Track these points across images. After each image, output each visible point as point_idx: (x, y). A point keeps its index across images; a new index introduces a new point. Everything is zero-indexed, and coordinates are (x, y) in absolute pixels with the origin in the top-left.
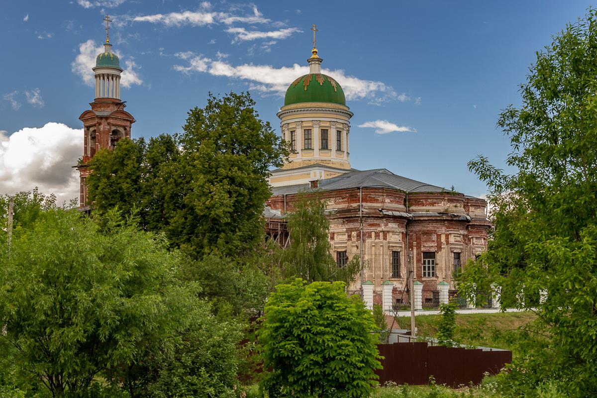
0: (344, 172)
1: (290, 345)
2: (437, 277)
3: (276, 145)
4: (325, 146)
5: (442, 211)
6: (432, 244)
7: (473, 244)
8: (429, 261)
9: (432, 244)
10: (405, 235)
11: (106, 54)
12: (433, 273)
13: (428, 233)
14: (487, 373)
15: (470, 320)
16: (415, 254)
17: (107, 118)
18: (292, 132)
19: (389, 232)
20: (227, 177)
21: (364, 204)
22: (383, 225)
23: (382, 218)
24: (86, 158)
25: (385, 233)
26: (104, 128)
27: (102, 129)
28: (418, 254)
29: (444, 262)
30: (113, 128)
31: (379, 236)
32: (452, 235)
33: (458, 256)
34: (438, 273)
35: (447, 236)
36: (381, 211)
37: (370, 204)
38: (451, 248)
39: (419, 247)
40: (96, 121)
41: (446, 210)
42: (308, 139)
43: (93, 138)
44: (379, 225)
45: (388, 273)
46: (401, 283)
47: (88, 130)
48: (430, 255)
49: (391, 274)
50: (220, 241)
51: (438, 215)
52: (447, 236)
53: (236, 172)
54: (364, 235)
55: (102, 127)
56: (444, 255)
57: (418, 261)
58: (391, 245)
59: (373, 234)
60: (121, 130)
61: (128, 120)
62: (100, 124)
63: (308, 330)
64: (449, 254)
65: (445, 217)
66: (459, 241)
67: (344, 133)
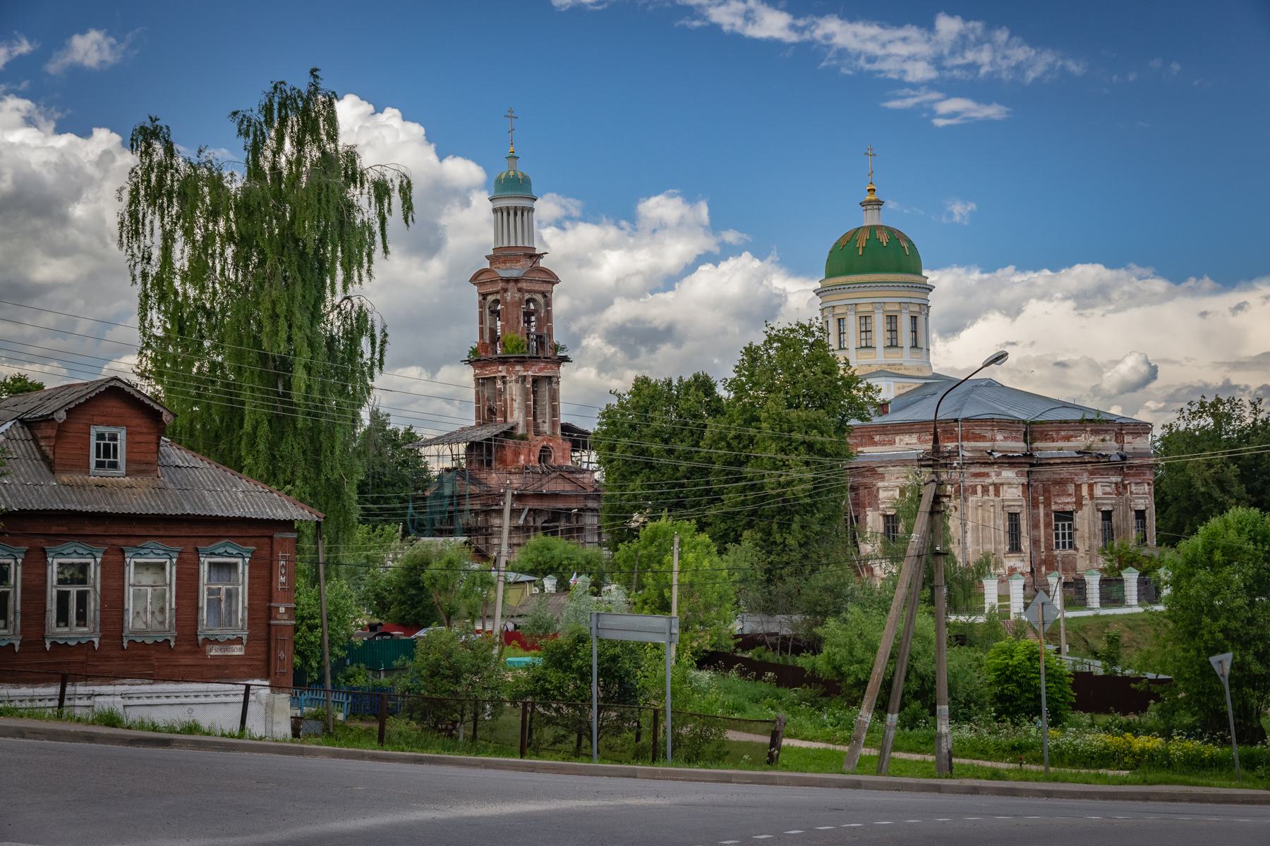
0: (924, 381)
1: (1012, 687)
2: (1076, 549)
3: (859, 390)
4: (893, 345)
5: (1082, 449)
6: (1069, 500)
7: (1131, 493)
8: (1063, 525)
9: (1069, 500)
10: (1027, 487)
11: (512, 173)
12: (1070, 544)
13: (1062, 483)
14: (1152, 702)
15: (1130, 623)
16: (1042, 514)
17: (517, 280)
18: (839, 320)
19: (1002, 484)
20: (804, 442)
21: (965, 444)
22: (993, 474)
23: (993, 464)
24: (482, 345)
25: (997, 487)
26: (513, 297)
27: (509, 298)
28: (1047, 515)
29: (1086, 526)
30: (527, 296)
31: (988, 491)
32: (1099, 485)
33: (1107, 515)
34: (1078, 544)
35: (1091, 487)
36: (990, 454)
37: (973, 444)
38: (1097, 505)
39: (1047, 504)
40: (500, 285)
41: (1089, 447)
42: (866, 331)
43: (495, 313)
44: (987, 475)
45: (1003, 546)
46: (1023, 561)
47: (485, 299)
48: (1065, 516)
49: (1007, 548)
50: (795, 526)
51: (1077, 455)
52: (1091, 487)
53: (815, 436)
54: (965, 490)
55: (508, 296)
56: (1086, 515)
57: (1047, 525)
58: (1006, 503)
59: (979, 489)
60: (539, 297)
61: (549, 282)
62: (505, 290)
63: (1025, 677)
64: (1093, 513)
65: (1087, 458)
66: (1110, 494)
67: (921, 320)
